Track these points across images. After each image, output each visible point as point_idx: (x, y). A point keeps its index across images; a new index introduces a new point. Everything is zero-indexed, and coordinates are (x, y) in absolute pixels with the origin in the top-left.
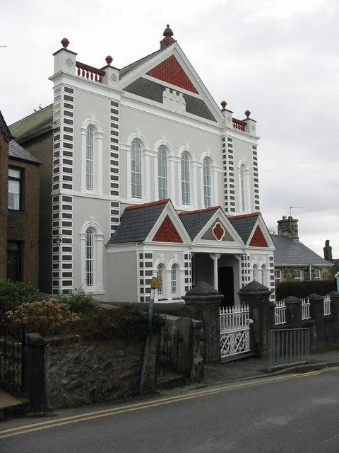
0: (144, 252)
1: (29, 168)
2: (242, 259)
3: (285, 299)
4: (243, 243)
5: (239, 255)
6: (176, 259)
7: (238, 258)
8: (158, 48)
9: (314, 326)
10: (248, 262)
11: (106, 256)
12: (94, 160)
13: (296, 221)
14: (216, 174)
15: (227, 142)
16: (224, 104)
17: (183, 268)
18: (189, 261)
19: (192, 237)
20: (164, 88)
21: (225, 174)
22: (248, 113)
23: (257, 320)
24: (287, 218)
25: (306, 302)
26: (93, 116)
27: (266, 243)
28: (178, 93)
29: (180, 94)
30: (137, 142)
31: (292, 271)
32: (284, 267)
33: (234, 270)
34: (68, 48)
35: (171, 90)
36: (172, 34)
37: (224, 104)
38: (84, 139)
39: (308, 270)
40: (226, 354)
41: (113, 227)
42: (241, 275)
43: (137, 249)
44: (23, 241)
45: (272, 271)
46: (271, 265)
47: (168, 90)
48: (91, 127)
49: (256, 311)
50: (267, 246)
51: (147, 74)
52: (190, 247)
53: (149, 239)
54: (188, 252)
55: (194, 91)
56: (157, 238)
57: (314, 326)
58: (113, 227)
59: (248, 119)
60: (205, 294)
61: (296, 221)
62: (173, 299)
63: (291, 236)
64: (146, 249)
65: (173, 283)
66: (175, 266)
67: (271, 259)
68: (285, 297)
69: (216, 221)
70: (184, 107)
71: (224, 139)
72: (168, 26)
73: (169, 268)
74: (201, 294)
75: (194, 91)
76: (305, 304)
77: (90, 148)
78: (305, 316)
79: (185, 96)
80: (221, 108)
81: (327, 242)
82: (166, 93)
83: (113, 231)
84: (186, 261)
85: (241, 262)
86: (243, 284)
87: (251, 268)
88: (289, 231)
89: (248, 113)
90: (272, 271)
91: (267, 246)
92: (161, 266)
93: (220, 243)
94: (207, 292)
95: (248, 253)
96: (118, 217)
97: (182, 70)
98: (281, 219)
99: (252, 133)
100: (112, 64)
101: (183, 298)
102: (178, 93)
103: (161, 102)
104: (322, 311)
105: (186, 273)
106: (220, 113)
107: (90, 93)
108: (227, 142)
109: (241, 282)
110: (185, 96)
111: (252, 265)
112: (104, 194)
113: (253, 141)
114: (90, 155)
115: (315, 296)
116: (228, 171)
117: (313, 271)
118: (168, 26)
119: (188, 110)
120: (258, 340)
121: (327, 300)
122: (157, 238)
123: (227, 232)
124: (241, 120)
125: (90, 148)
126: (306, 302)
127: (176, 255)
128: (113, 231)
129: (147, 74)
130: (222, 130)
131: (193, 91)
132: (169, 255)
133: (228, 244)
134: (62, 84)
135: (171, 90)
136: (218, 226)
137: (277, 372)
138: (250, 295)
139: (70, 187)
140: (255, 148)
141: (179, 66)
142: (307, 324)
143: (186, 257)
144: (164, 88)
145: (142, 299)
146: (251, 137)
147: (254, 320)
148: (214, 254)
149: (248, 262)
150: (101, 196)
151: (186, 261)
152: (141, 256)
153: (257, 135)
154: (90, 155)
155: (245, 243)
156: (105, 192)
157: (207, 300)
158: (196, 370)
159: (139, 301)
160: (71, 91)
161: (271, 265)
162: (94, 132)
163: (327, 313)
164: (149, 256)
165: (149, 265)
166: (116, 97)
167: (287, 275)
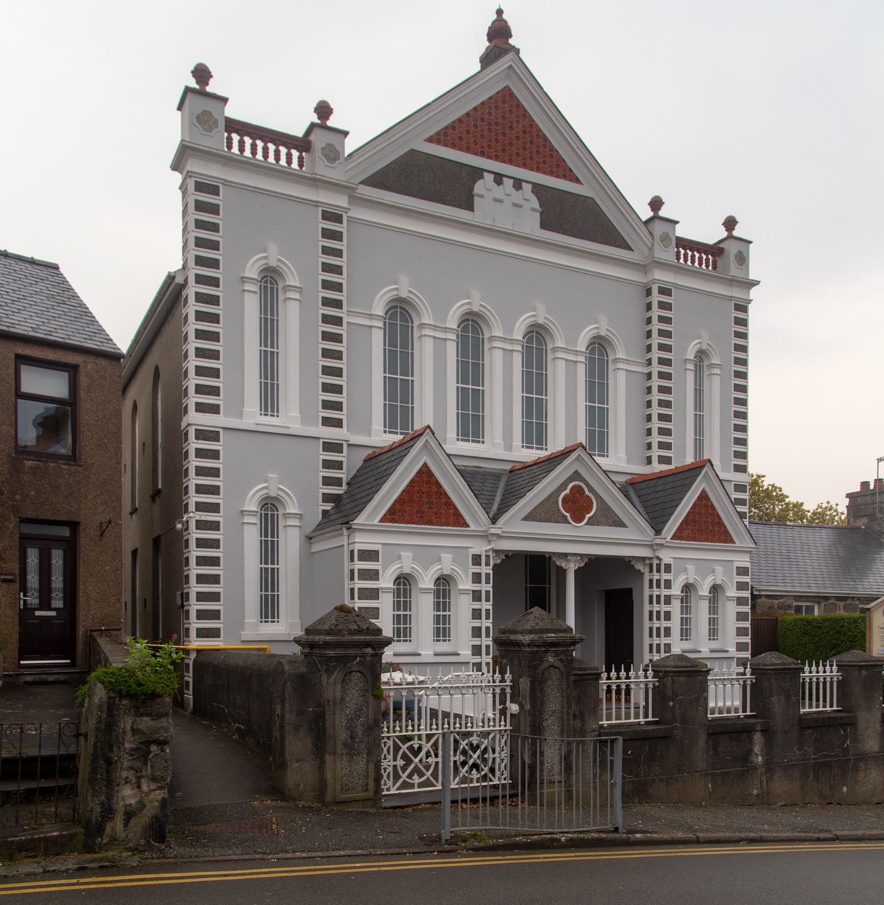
0: (357, 547)
1: (88, 366)
2: (651, 571)
3: (838, 657)
4: (650, 532)
5: (643, 559)
6: (719, 576)
7: (639, 566)
8: (477, 67)
9: (758, 737)
10: (665, 576)
11: (307, 559)
12: (706, 413)
14: (622, 377)
15: (656, 298)
17: (732, 592)
18: (485, 570)
20: (477, 173)
21: (649, 376)
23: (528, 707)
26: (273, 248)
27: (726, 532)
28: (518, 184)
29: (524, 185)
32: (826, 598)
34: (330, 123)
35: (499, 179)
37: (656, 204)
38: (690, 377)
40: (420, 785)
41: (327, 498)
44: (79, 522)
45: (740, 601)
46: (741, 586)
47: (489, 177)
48: (701, 354)
49: (525, 683)
51: (430, 140)
52: (486, 537)
54: (480, 548)
55: (568, 175)
56: (395, 514)
57: (758, 737)
58: (327, 498)
62: (436, 655)
64: (363, 541)
65: (713, 622)
66: (716, 589)
67: (742, 571)
71: (649, 292)
72: (500, 12)
73: (704, 591)
75: (568, 175)
77: (699, 394)
79: (537, 189)
83: (328, 507)
84: (476, 569)
89: (730, 223)
90: (740, 601)
92: (688, 588)
93: (581, 530)
95: (667, 557)
96: (343, 475)
98: (857, 488)
99: (734, 271)
100: (662, 213)
101: (297, 641)
102: (518, 184)
103: (470, 207)
105: (477, 596)
108: (656, 298)
110: (537, 189)
112: (628, 462)
113: (737, 293)
114: (699, 404)
116: (656, 368)
118: (500, 12)
119: (545, 225)
122: (395, 514)
124: (711, 242)
125: (699, 394)
127: (719, 569)
128: (328, 507)
129: (430, 140)
130: (644, 268)
131: (564, 177)
132: (705, 567)
134: (654, 281)
135: (499, 179)
136: (577, 490)
139: (214, 409)
141: (525, 115)
143: (476, 559)
144: (477, 173)
146: (733, 282)
147: (521, 706)
148: (565, 555)
149: (665, 576)
150: (296, 428)
151: (476, 569)
153: (752, 276)
154: (699, 404)
156: (304, 421)
160: (214, 190)
161: (741, 586)
162: (706, 363)
164: (370, 555)
166: (339, 201)
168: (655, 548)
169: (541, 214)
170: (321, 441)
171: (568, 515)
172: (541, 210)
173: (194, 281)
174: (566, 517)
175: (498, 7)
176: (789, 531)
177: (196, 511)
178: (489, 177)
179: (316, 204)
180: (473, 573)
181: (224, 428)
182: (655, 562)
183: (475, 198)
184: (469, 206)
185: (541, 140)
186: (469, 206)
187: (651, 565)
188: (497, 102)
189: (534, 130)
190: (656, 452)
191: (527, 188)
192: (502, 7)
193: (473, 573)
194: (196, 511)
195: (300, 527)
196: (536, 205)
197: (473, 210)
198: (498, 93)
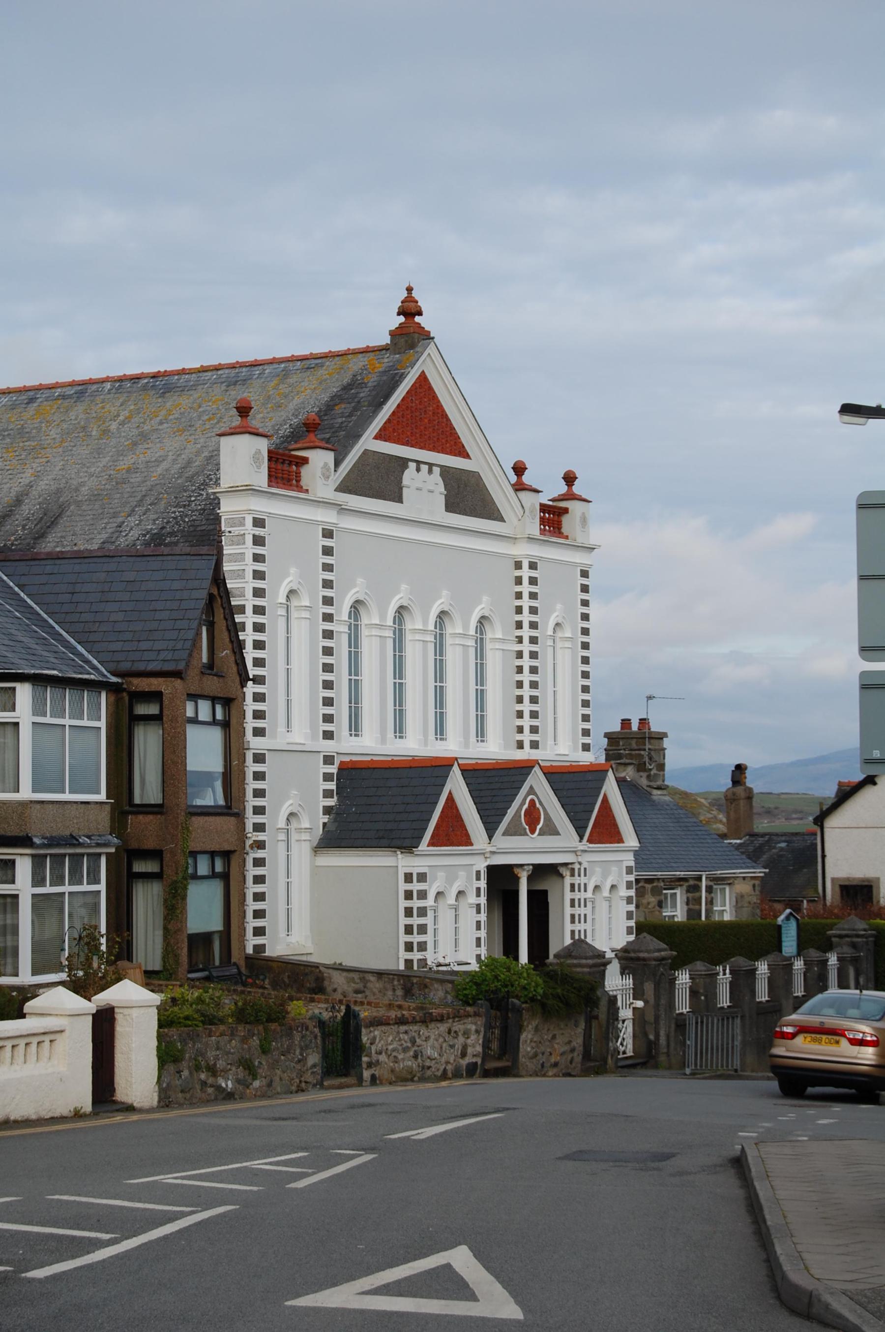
2: (573, 875)
4: (577, 838)
11: (315, 871)
13: (661, 737)
16: (519, 469)
19: (491, 834)
20: (403, 463)
22: (570, 479)
23: (652, 1001)
24: (635, 727)
25: (724, 974)
30: (357, 607)
31: (656, 891)
33: (551, 899)
36: (420, 313)
37: (519, 469)
39: (697, 888)
42: (568, 911)
43: (404, 863)
49: (649, 987)
50: (621, 840)
53: (423, 846)
59: (570, 496)
60: (586, 958)
61: (661, 737)
63: (644, 782)
68: (690, 963)
69: (528, 794)
70: (441, 501)
71: (518, 565)
74: (581, 958)
76: (724, 977)
78: (724, 1000)
80: (514, 478)
81: (542, 492)
82: (409, 476)
85: (568, 880)
86: (573, 932)
87: (589, 894)
88: (641, 767)
89: (570, 479)
91: (621, 840)
94: (591, 954)
97: (439, 406)
98: (617, 727)
104: (753, 992)
106: (510, 491)
107: (294, 519)
109: (568, 927)
111: (590, 888)
113: (580, 558)
115: (741, 961)
116: (526, 647)
117: (709, 889)
118: (409, 290)
120: (652, 1037)
121: (763, 968)
123: (548, 818)
126: (724, 974)
133: (549, 842)
136: (532, 802)
137: (697, 1076)
138: (638, 959)
140: (585, 574)
141: (435, 398)
142: (726, 1015)
145: (408, 963)
147: (646, 1002)
150: (310, 746)
152: (408, 878)
153: (592, 541)
155: (581, 838)
156: (314, 737)
157: (591, 966)
158: (612, 1058)
159: (402, 967)
163: (762, 995)
164: (422, 877)
165: (423, 895)
166: (328, 517)
167: (645, 901)
168: (579, 853)
169: (446, 496)
170: (322, 755)
171: (527, 827)
172: (445, 493)
173: (252, 612)
174: (525, 829)
175: (408, 285)
176: (195, 624)
177: (254, 831)
178: (412, 466)
179: (315, 523)
180: (627, 882)
181: (268, 750)
182: (576, 866)
183: (404, 489)
184: (398, 498)
185: (445, 420)
186: (398, 498)
187: (573, 870)
188: (416, 389)
189: (440, 411)
190: (527, 737)
191: (437, 470)
192: (411, 285)
193: (627, 882)
194: (254, 831)
195: (310, 841)
196: (442, 489)
197: (402, 503)
198: (463, 446)
